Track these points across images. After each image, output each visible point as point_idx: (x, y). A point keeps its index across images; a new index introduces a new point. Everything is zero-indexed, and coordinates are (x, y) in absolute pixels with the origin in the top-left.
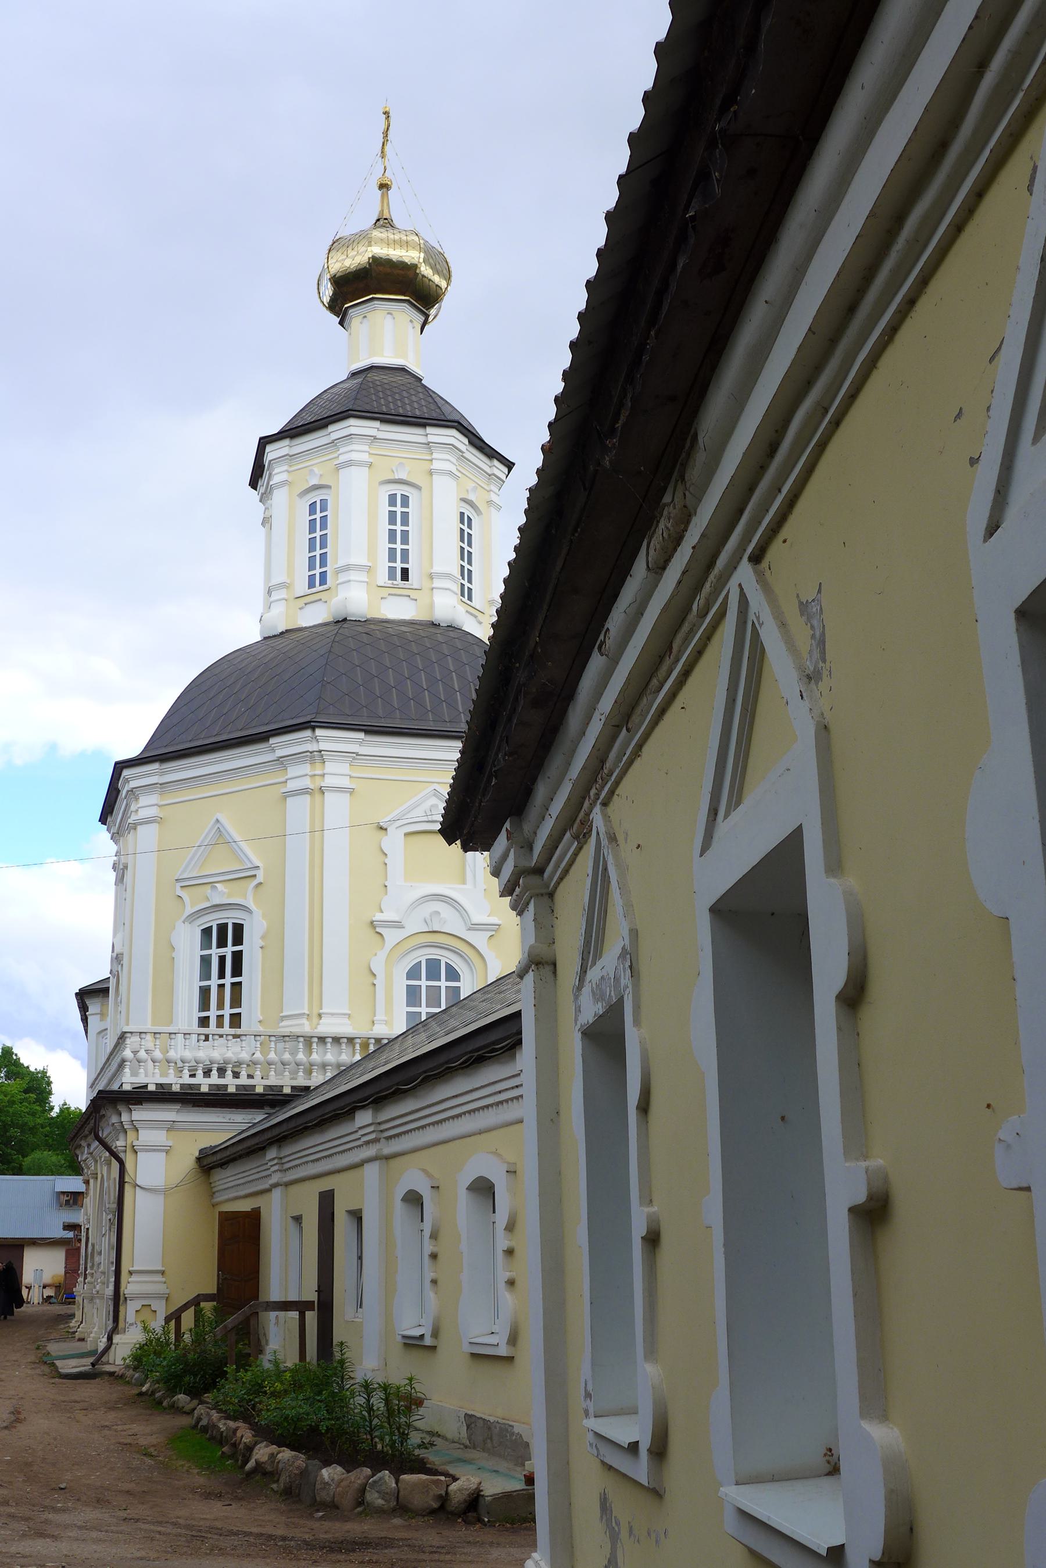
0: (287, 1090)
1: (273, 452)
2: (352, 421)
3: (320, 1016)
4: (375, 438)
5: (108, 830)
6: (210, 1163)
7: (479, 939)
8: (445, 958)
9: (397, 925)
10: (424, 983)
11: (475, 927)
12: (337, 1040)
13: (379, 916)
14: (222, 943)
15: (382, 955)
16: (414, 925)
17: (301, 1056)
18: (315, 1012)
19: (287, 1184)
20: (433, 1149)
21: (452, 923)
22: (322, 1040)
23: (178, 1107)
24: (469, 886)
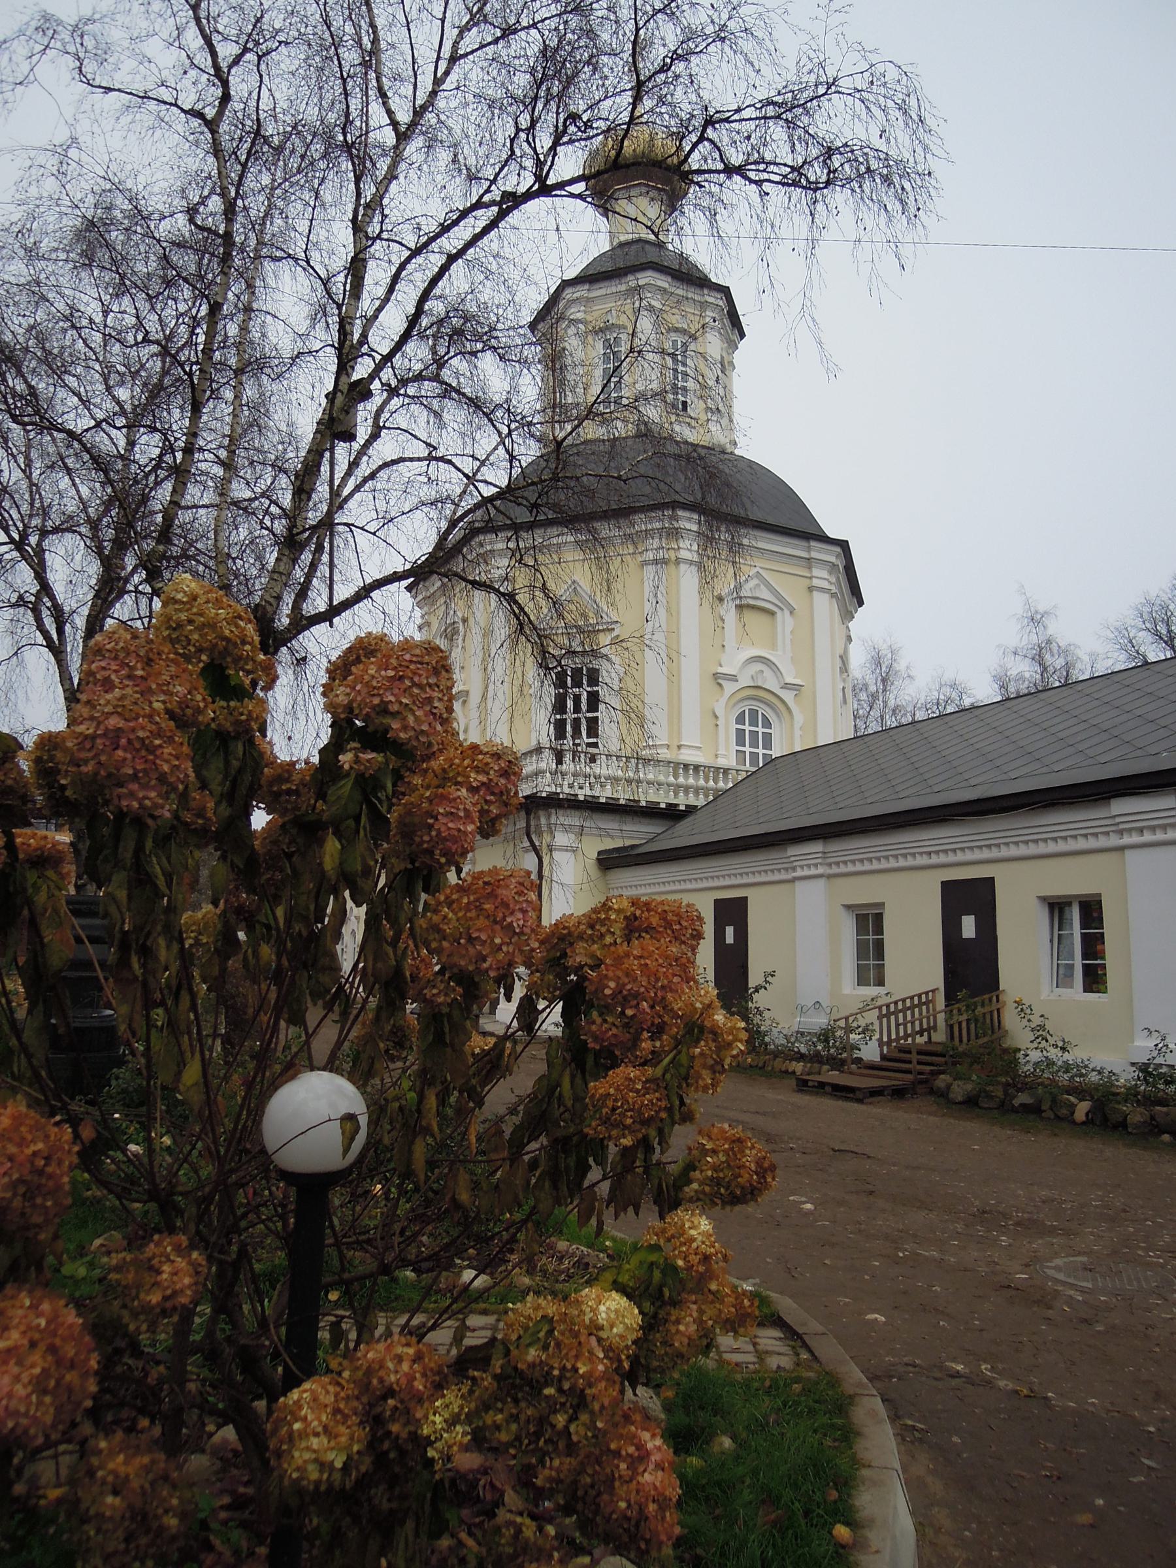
0: (682, 808)
1: (569, 293)
2: (649, 273)
3: (679, 747)
4: (588, 300)
5: (415, 597)
6: (609, 862)
7: (788, 696)
8: (762, 709)
9: (733, 678)
10: (747, 728)
11: (787, 686)
12: (697, 768)
13: (720, 670)
14: (578, 684)
15: (723, 701)
16: (744, 681)
17: (702, 782)
18: (676, 743)
19: (829, 877)
20: (1158, 849)
21: (772, 684)
22: (686, 766)
23: (618, 817)
24: (780, 653)
